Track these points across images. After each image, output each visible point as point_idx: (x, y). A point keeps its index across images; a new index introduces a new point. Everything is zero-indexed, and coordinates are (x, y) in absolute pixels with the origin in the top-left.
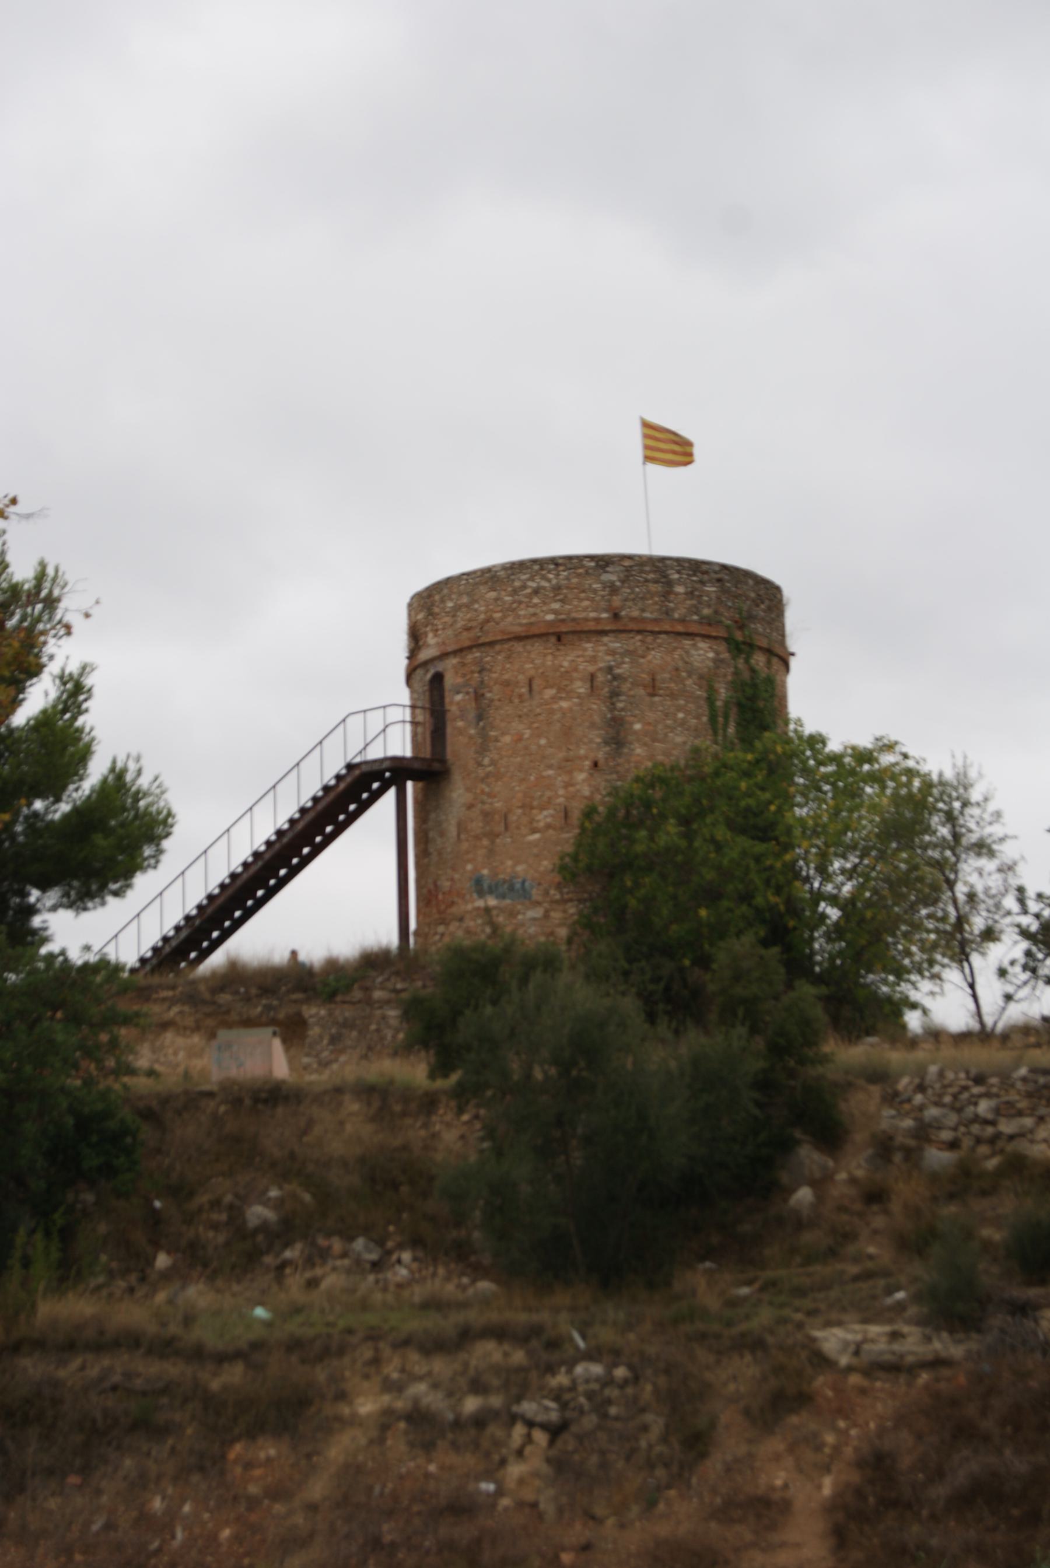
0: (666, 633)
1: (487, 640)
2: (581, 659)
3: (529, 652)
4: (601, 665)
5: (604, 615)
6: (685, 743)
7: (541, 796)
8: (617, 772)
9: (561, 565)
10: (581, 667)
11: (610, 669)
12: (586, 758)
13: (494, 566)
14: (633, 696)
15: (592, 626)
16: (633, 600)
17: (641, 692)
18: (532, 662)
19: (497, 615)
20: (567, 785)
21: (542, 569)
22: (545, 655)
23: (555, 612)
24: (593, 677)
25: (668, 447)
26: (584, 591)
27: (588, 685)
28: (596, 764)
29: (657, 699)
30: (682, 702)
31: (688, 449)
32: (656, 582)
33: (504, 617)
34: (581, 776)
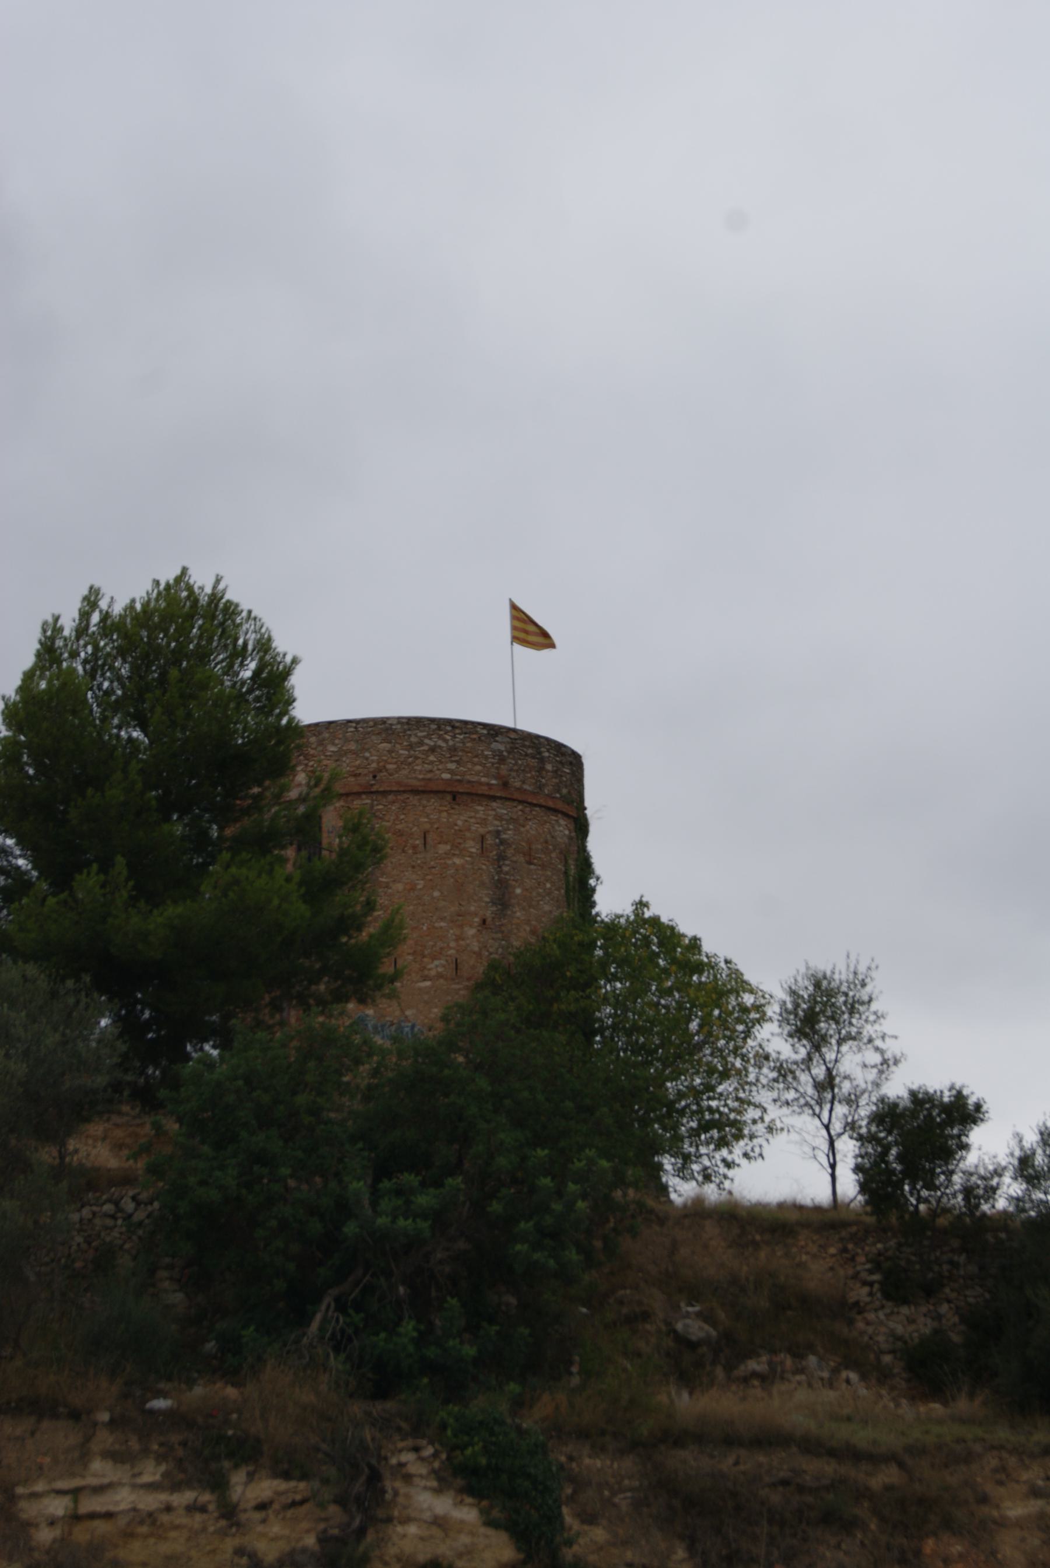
0: (540, 806)
1: (381, 789)
2: (472, 820)
3: (425, 807)
4: (491, 828)
5: (494, 782)
6: (551, 912)
7: (434, 946)
8: (502, 932)
9: (457, 728)
10: (473, 828)
11: (498, 833)
12: (476, 915)
13: (388, 718)
14: (515, 862)
15: (484, 790)
16: (517, 771)
17: (521, 859)
18: (427, 816)
19: (390, 767)
20: (459, 938)
21: (439, 728)
22: (441, 812)
23: (451, 772)
24: (483, 838)
25: (529, 632)
26: (476, 756)
27: (479, 846)
28: (484, 921)
29: (532, 867)
30: (549, 873)
31: (517, 634)
32: (533, 757)
33: (398, 770)
34: (472, 932)
